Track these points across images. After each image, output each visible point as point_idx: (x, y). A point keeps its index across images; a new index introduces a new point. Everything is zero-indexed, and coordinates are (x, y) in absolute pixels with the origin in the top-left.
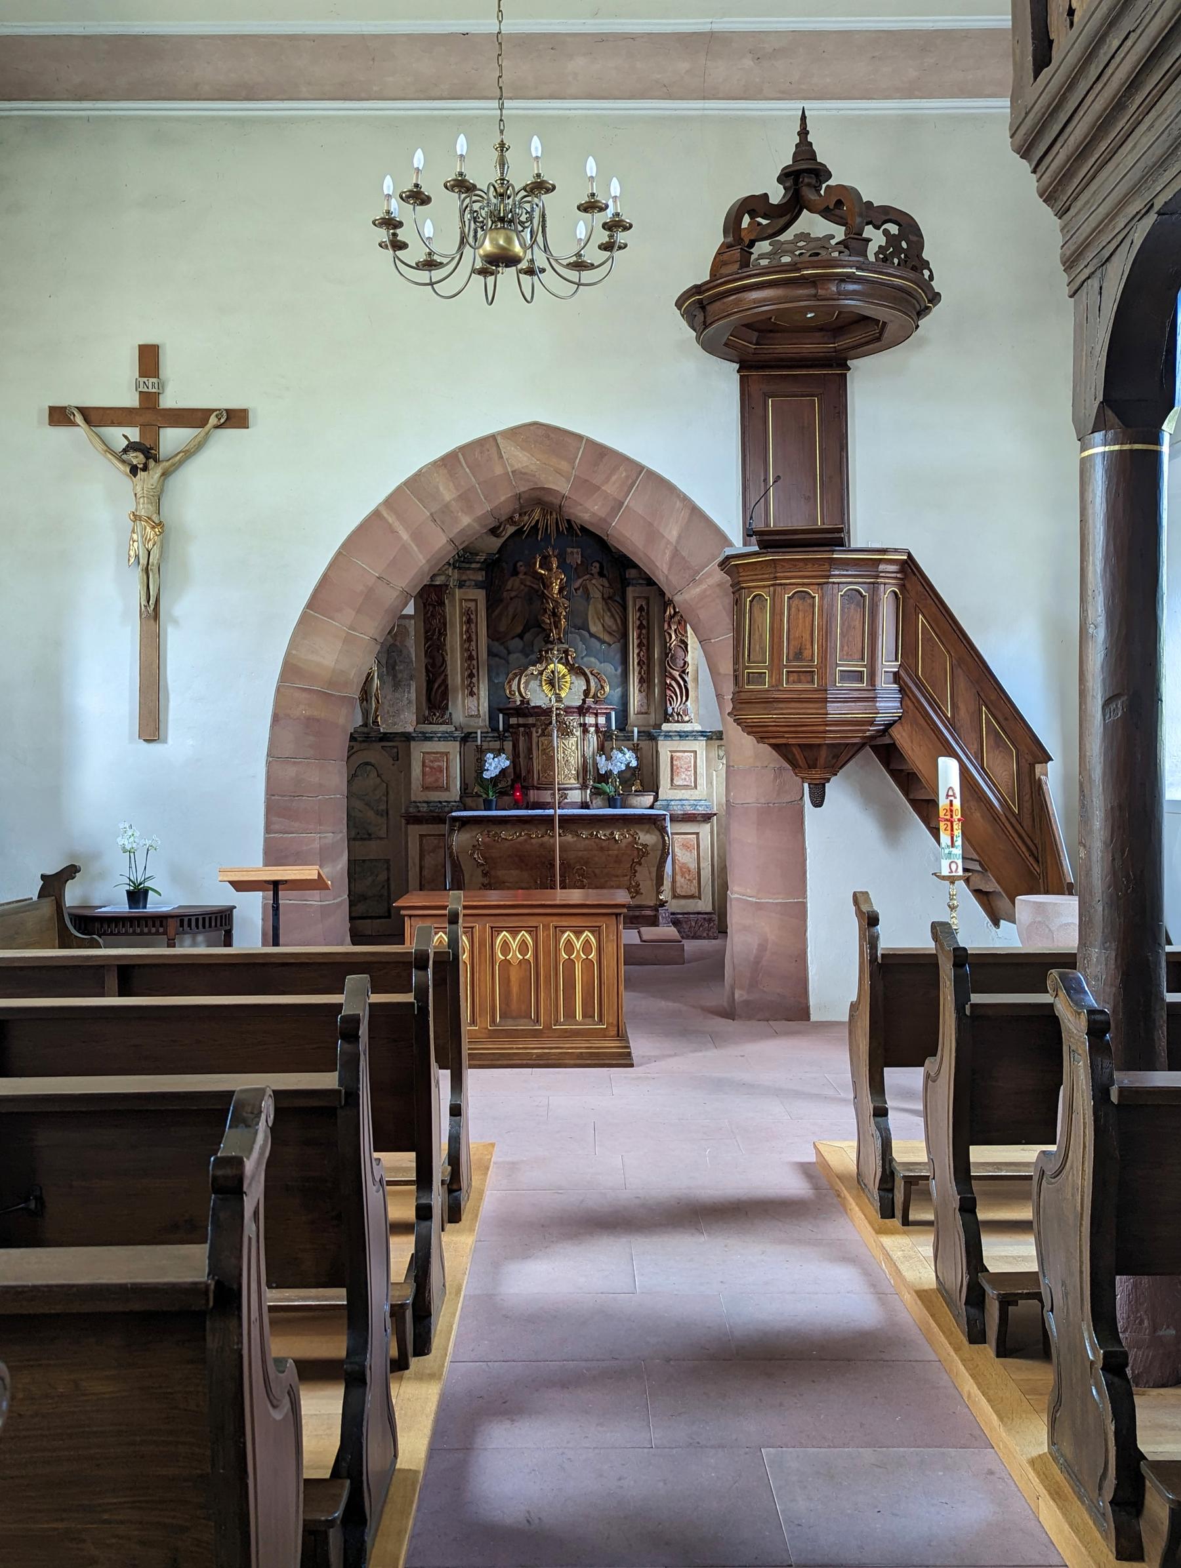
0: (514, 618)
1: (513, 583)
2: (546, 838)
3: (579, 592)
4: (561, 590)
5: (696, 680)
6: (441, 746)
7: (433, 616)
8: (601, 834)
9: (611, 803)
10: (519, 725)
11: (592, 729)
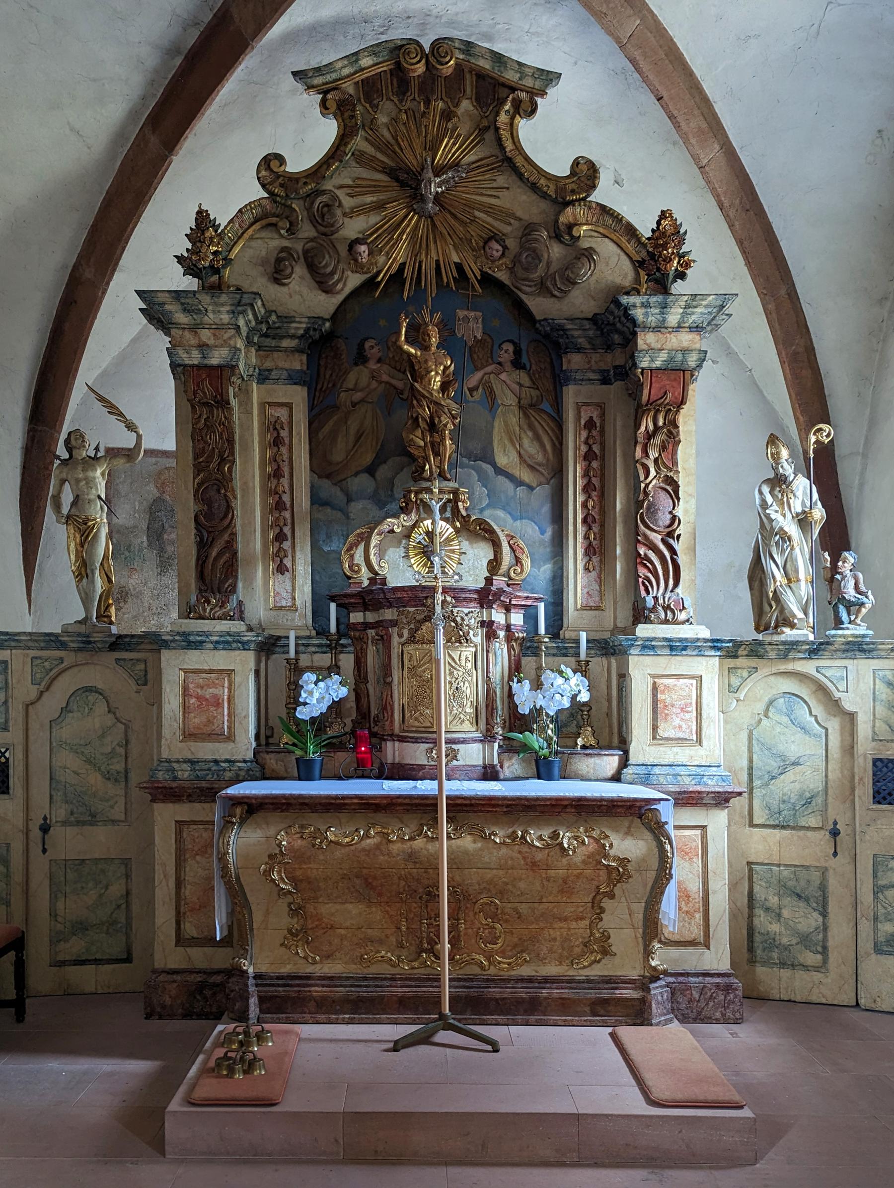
0: (358, 438)
1: (358, 377)
2: (419, 843)
3: (478, 395)
4: (444, 387)
5: (692, 550)
6: (219, 660)
7: (195, 393)
8: (533, 835)
9: (543, 769)
10: (366, 626)
11: (502, 634)
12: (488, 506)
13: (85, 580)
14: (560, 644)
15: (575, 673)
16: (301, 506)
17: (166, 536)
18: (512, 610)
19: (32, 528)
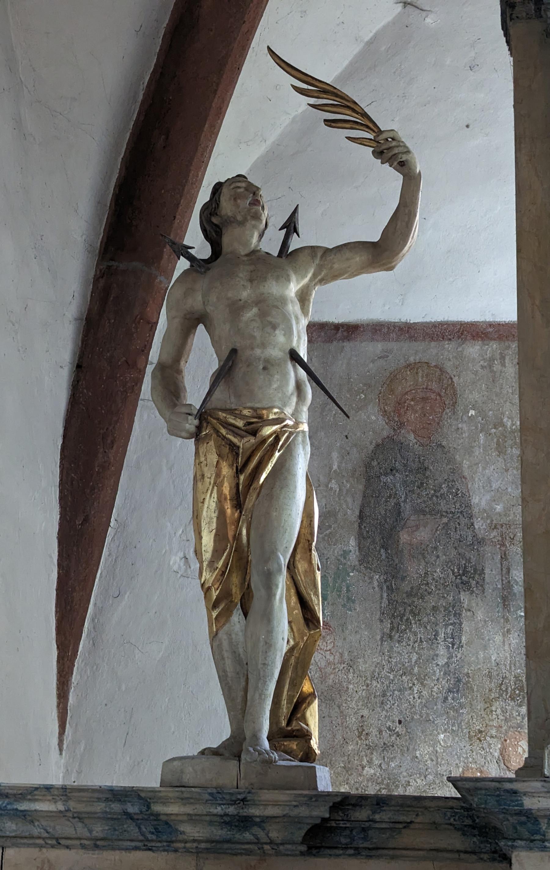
13: (237, 616)
17: (404, 537)
19: (86, 520)
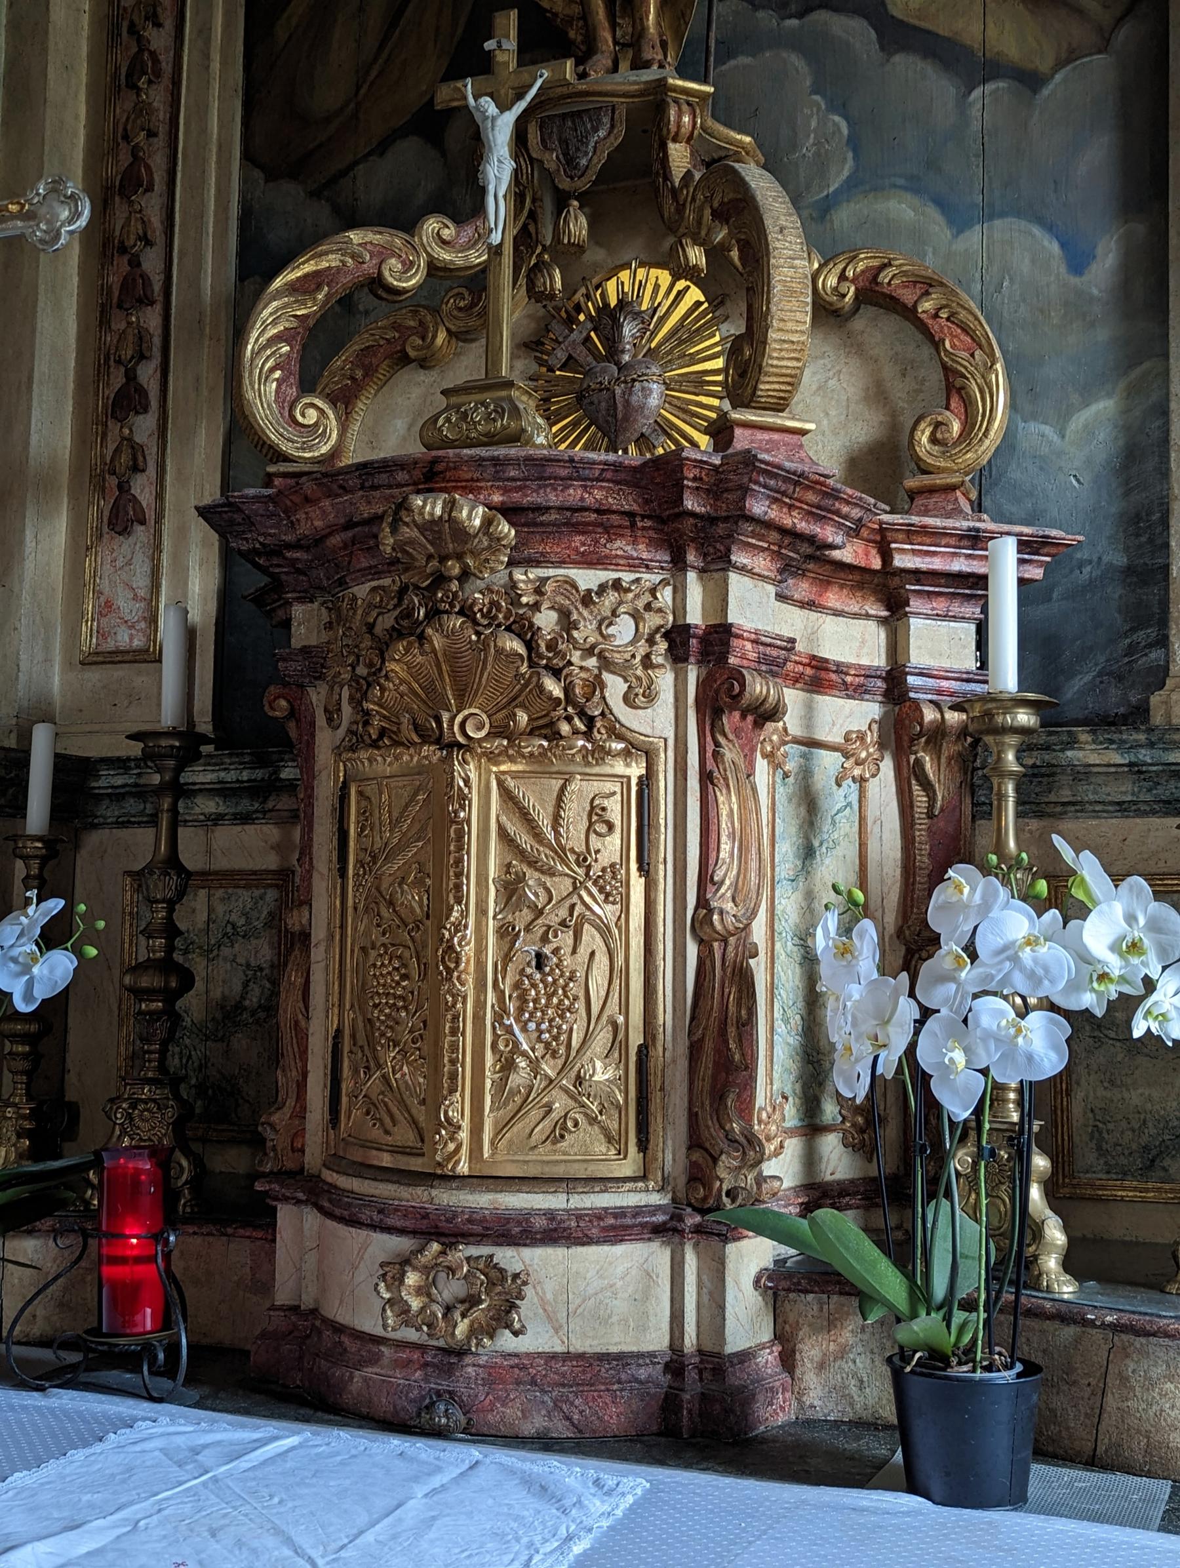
12: (852, 186)
14: (1145, 755)
15: (1117, 878)
16: (194, 282)
18: (915, 604)
